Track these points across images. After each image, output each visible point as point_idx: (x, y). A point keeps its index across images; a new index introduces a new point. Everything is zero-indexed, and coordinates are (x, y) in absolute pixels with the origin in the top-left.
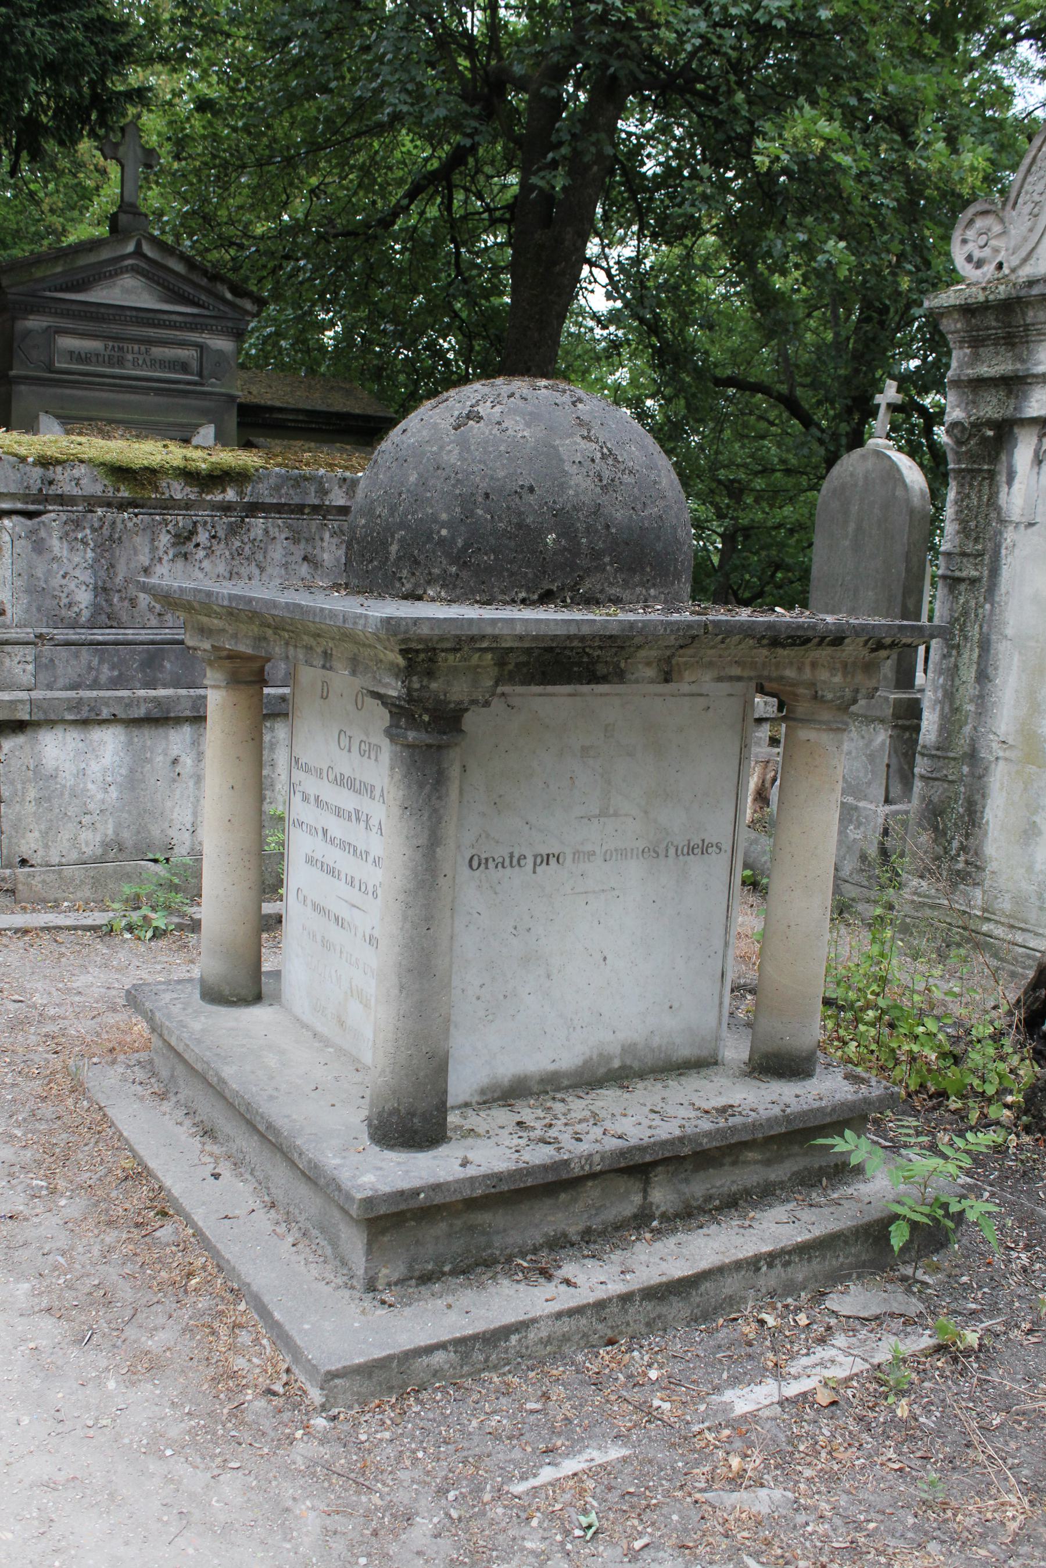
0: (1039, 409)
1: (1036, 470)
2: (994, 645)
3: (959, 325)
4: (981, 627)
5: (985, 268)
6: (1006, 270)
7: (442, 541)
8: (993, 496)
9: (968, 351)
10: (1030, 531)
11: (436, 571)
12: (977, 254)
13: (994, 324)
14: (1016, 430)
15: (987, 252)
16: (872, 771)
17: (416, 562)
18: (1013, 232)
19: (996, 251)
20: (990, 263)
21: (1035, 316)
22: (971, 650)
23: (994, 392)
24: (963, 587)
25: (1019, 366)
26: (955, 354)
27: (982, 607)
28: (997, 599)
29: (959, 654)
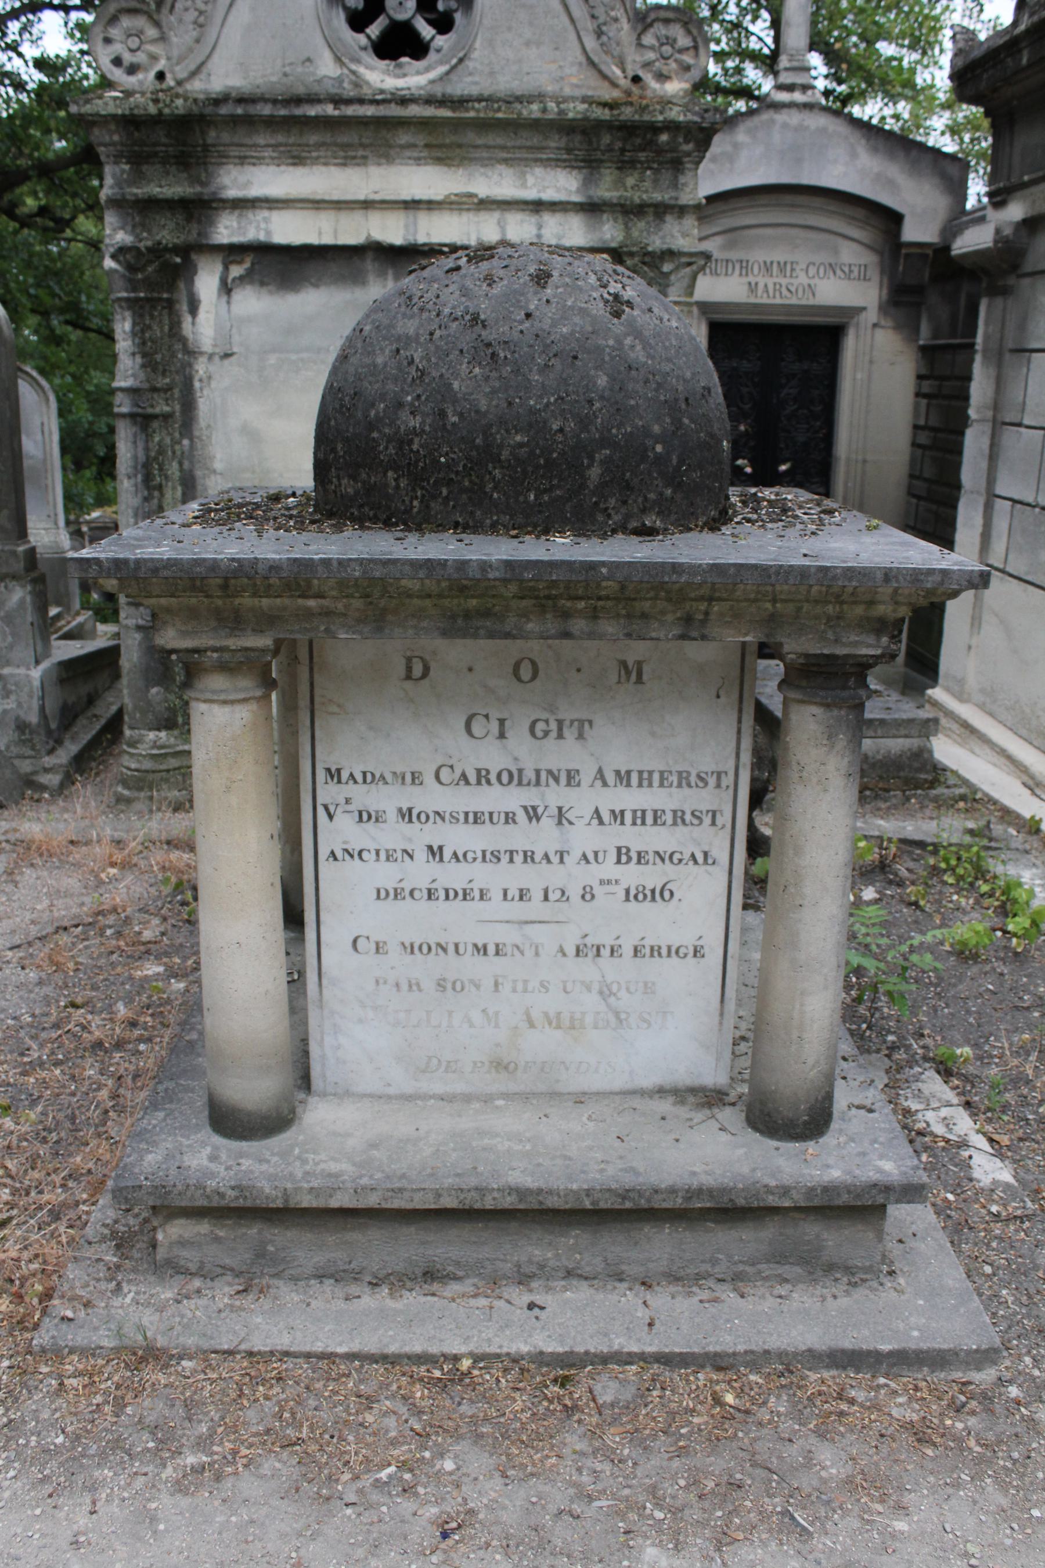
0: (229, 236)
1: (225, 298)
2: (199, 482)
3: (116, 138)
4: (181, 464)
5: (140, 76)
6: (170, 81)
7: (658, 458)
8: (176, 325)
9: (127, 167)
10: (226, 362)
11: (652, 496)
12: (128, 58)
13: (164, 140)
14: (194, 256)
15: (140, 58)
16: (13, 634)
17: (628, 487)
18: (175, 40)
19: (154, 58)
20: (146, 70)
21: (218, 137)
22: (174, 488)
23: (169, 215)
24: (155, 424)
25: (198, 189)
26: (108, 170)
27: (180, 443)
28: (196, 433)
29: (162, 495)
